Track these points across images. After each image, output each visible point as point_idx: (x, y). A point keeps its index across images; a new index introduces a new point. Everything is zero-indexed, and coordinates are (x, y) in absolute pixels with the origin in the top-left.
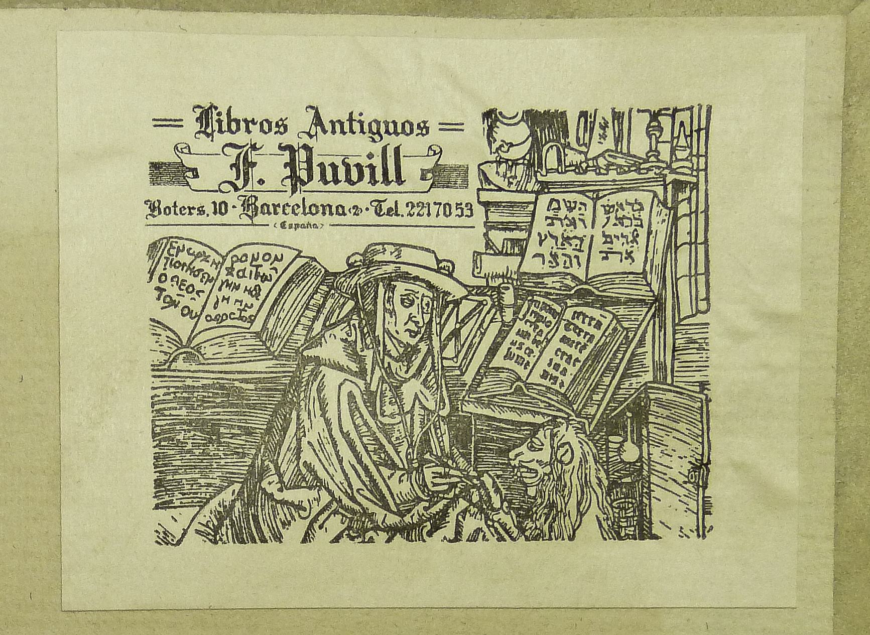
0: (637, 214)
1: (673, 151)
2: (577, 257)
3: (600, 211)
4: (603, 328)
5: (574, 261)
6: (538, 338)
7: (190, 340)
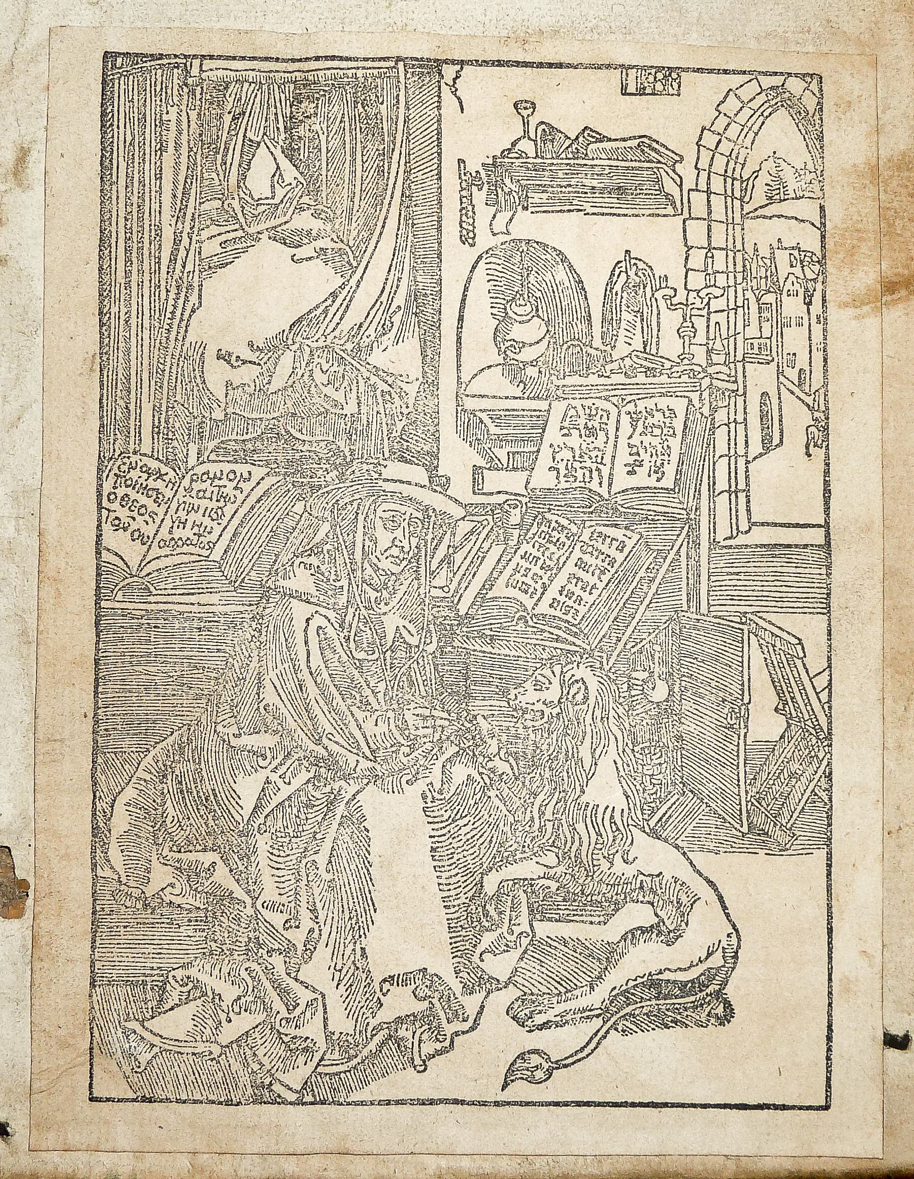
0: (668, 421)
1: (709, 352)
2: (598, 470)
3: (625, 420)
4: (626, 551)
5: (595, 474)
6: (548, 562)
7: (140, 568)
